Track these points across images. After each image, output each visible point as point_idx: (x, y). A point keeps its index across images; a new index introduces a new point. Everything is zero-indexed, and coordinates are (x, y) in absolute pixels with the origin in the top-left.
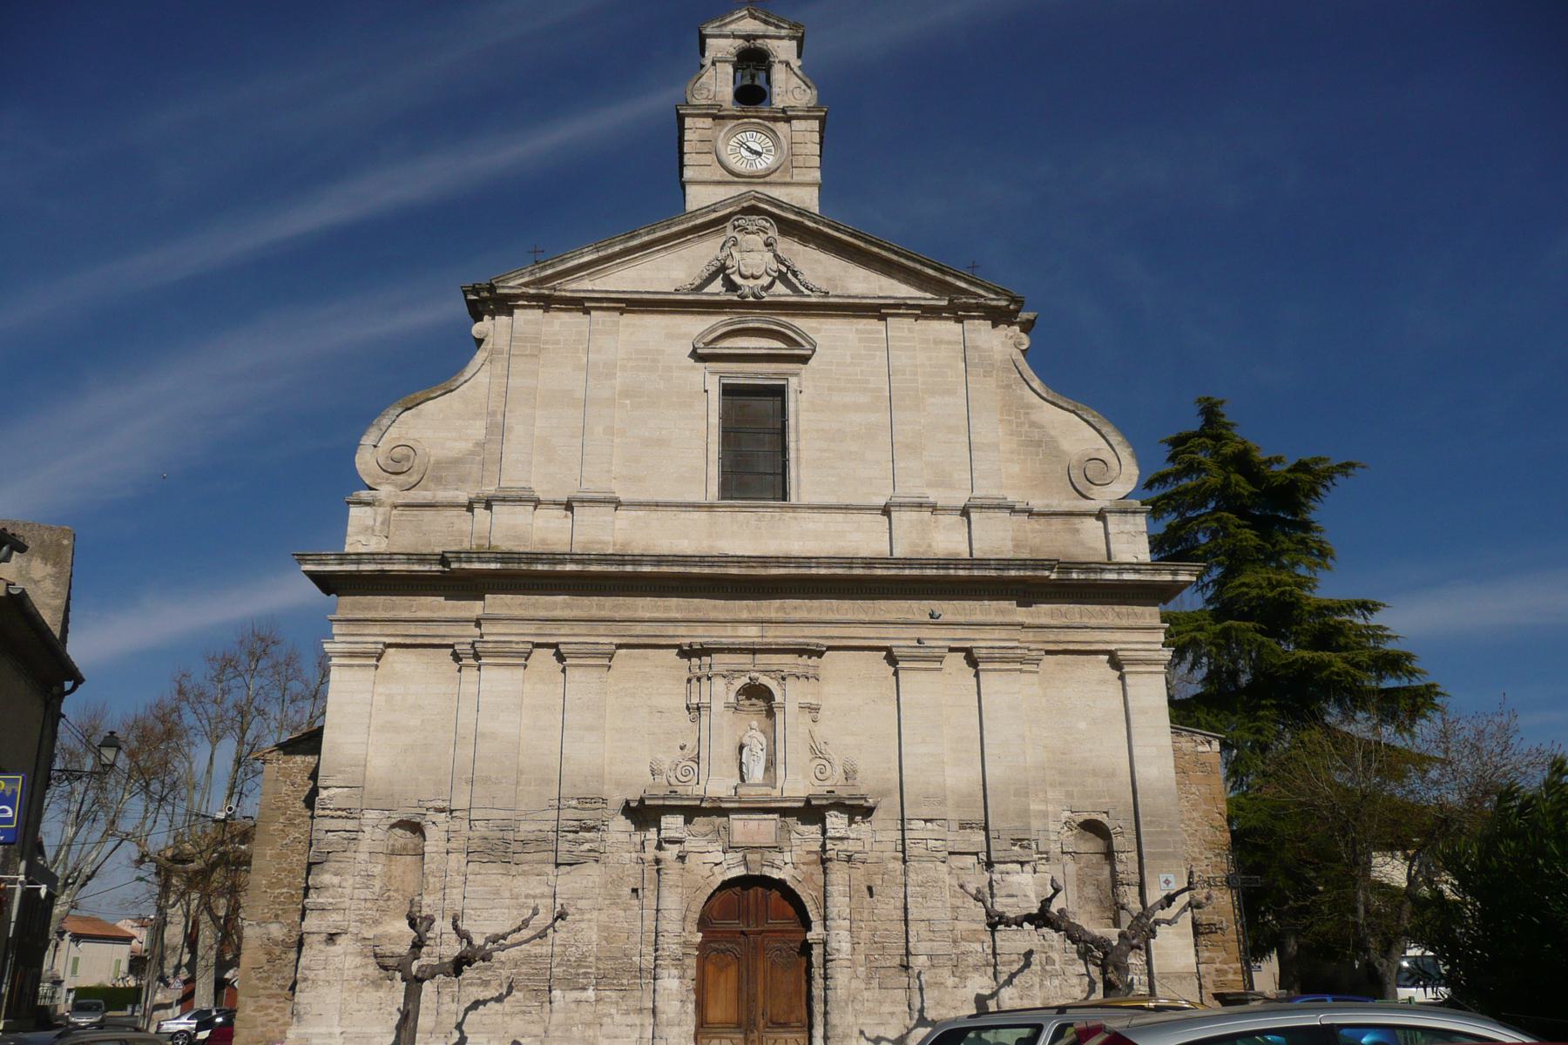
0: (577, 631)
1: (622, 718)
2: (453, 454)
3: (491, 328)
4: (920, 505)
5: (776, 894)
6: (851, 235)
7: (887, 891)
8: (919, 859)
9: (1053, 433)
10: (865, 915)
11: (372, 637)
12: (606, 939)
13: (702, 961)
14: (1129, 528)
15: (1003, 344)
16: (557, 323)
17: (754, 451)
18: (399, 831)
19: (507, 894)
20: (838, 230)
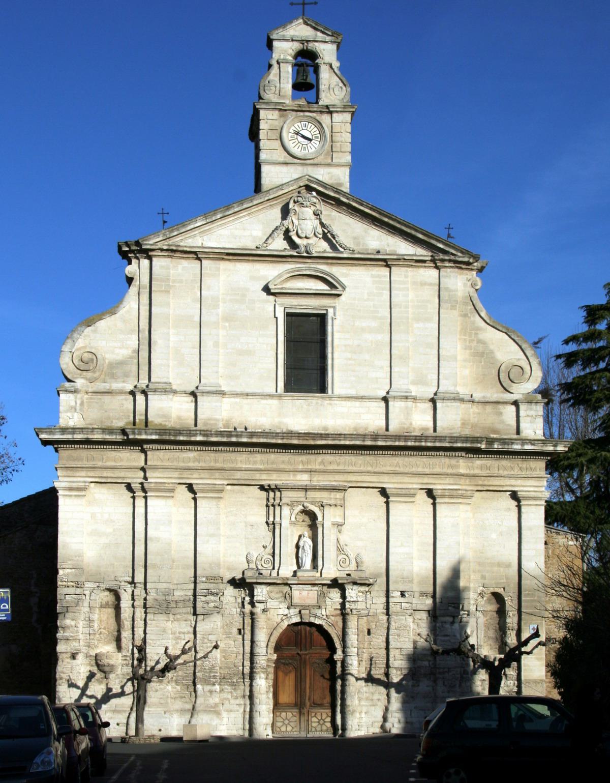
0: (202, 476)
1: (231, 530)
2: (120, 358)
3: (137, 268)
4: (407, 398)
5: (314, 629)
6: (371, 209)
7: (379, 631)
8: (397, 614)
9: (492, 347)
10: (366, 645)
11: (80, 478)
12: (224, 657)
13: (276, 669)
14: (532, 413)
15: (465, 285)
16: (180, 267)
17: (306, 356)
18: (107, 593)
19: (170, 632)
20: (362, 205)
